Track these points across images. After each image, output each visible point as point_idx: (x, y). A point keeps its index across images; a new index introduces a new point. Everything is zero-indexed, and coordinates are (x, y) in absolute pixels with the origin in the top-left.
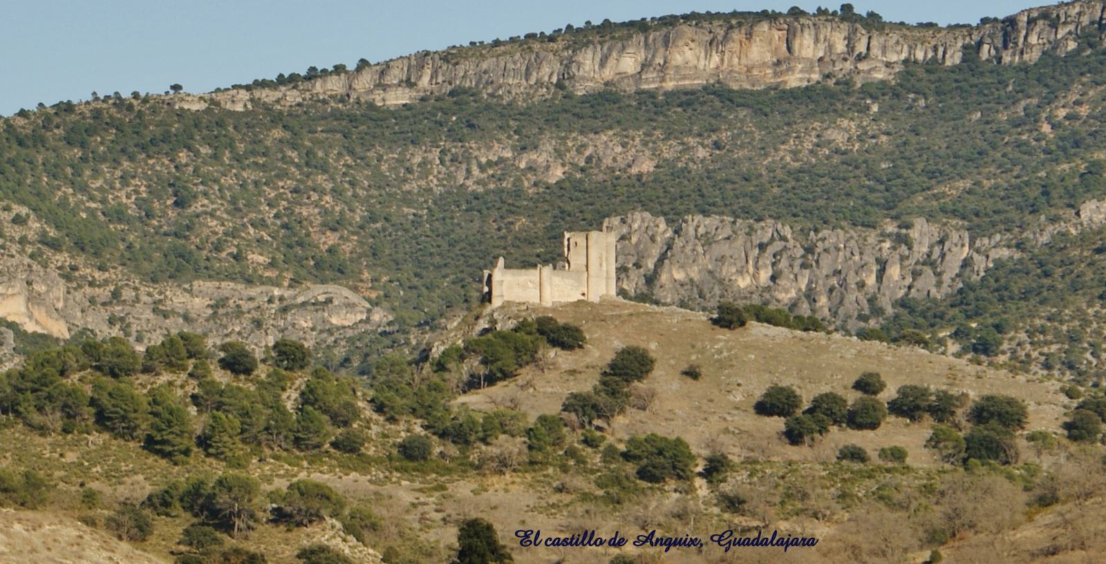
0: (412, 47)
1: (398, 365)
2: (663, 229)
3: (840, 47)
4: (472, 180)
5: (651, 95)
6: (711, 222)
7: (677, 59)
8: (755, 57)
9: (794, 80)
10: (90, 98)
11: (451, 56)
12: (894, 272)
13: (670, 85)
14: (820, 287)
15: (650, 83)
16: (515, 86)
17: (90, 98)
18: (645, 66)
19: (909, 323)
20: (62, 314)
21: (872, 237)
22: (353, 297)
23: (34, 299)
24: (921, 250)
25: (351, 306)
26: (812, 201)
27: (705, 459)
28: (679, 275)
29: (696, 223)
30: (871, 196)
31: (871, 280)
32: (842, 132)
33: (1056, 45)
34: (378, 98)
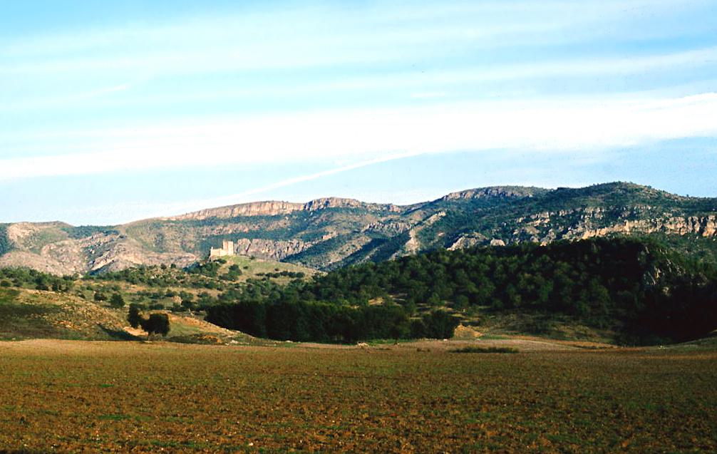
0: (204, 208)
1: (224, 262)
2: (249, 241)
3: (281, 207)
4: (215, 233)
5: (248, 217)
6: (258, 240)
7: (252, 210)
8: (266, 209)
9: (273, 214)
10: (686, 196)
11: (212, 210)
12: (290, 249)
13: (251, 215)
14: (277, 252)
15: (247, 214)
16: (222, 215)
17: (686, 196)
18: (247, 211)
19: (288, 259)
20: (141, 260)
21: (286, 242)
22: (193, 255)
23: (136, 257)
24: (295, 245)
25: (193, 257)
26: (276, 236)
27: (174, 304)
28: (252, 250)
29: (255, 241)
30: (290, 234)
31: (286, 251)
32: (281, 223)
33: (319, 206)
34: (198, 218)
